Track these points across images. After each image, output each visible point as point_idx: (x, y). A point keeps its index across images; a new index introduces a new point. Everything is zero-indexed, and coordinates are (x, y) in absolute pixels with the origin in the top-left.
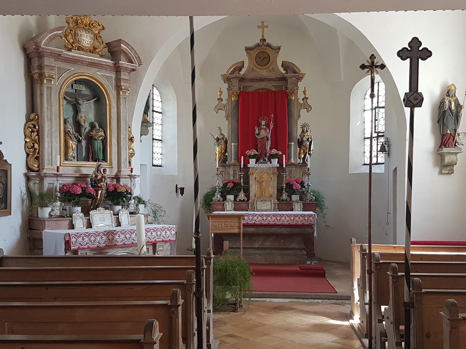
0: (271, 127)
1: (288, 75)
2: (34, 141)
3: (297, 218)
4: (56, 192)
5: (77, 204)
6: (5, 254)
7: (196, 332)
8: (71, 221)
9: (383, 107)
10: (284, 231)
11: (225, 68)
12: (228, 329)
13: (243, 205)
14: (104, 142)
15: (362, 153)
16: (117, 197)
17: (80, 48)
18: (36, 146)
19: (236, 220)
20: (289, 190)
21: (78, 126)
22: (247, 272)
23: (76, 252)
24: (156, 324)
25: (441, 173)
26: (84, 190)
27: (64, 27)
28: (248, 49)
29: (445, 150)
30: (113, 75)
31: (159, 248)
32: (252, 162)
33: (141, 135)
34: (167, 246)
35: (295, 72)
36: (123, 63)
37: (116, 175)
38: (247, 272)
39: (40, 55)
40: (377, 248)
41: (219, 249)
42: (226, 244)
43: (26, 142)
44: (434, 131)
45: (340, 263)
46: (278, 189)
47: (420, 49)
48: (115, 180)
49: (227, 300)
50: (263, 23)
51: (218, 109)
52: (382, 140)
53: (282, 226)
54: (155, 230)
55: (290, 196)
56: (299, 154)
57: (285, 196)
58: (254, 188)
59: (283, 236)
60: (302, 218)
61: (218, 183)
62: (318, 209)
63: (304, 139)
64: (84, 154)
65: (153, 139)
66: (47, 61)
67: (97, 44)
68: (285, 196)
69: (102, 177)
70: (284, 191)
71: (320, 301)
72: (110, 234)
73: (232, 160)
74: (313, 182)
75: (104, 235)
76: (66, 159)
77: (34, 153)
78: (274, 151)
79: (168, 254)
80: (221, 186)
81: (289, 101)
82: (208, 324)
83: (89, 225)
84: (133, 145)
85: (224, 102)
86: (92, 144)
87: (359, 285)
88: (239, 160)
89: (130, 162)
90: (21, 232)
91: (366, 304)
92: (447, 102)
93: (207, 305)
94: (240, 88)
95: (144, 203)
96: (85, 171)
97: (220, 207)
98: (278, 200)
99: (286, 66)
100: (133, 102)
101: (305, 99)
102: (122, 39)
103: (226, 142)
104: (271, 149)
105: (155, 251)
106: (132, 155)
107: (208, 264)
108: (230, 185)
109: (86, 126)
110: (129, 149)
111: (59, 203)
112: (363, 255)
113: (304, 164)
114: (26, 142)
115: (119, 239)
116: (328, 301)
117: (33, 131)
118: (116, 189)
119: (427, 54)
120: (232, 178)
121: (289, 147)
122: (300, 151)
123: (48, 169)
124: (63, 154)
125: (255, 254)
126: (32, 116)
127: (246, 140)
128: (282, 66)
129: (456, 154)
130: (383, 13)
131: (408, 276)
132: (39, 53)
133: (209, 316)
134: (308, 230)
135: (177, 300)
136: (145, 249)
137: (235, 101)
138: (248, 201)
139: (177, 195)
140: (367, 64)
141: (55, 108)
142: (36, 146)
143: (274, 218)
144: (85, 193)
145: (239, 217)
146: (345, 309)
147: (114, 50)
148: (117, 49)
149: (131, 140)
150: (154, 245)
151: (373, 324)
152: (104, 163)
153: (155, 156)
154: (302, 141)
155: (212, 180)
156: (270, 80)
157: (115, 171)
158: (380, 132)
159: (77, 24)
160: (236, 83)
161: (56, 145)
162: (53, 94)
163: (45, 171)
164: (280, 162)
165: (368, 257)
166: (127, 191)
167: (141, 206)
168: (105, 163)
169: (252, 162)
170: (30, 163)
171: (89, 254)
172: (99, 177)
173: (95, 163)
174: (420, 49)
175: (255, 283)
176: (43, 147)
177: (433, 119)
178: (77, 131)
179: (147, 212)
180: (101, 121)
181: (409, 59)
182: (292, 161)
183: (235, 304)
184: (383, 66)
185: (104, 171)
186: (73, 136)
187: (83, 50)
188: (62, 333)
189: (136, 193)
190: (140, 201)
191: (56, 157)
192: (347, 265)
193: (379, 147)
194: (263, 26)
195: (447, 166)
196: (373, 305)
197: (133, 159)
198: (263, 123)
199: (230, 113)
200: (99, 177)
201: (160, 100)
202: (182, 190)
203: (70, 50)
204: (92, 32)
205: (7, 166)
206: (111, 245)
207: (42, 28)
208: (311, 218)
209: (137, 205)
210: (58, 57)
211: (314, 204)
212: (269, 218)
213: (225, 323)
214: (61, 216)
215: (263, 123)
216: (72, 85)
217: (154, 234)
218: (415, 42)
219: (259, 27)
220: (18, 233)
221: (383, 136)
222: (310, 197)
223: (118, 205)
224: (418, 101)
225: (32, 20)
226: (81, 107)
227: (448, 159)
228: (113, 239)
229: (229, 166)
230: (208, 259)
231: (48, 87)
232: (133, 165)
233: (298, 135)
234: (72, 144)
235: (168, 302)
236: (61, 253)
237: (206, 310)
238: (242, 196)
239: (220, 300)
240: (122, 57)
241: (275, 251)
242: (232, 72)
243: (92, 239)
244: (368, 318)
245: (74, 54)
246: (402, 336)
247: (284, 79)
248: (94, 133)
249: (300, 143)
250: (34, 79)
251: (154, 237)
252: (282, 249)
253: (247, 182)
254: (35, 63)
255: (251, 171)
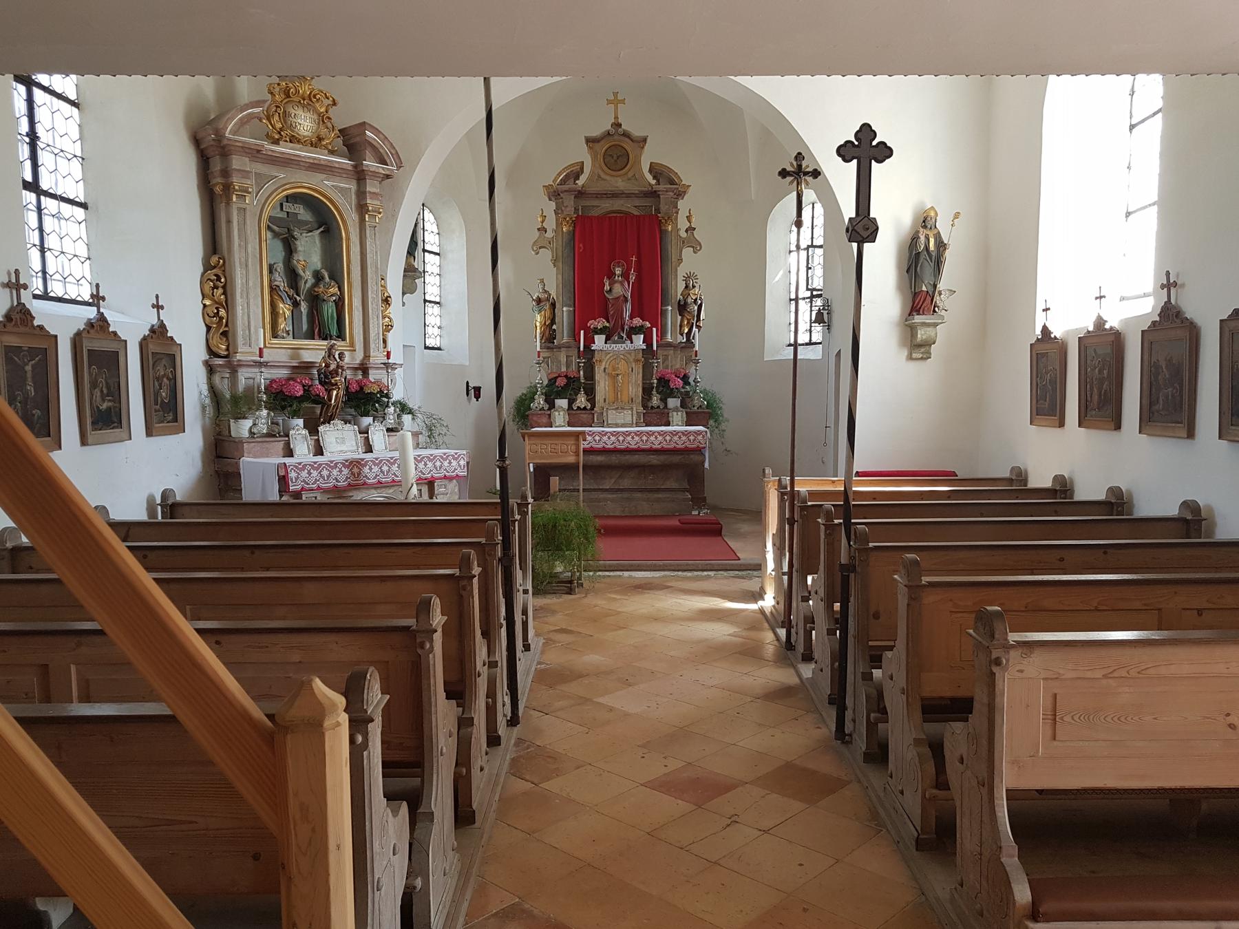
0: (632, 278)
1: (661, 187)
2: (218, 305)
3: (676, 438)
4: (259, 392)
5: (296, 414)
6: (178, 498)
7: (504, 623)
8: (288, 444)
9: (821, 247)
10: (654, 459)
11: (551, 174)
12: (559, 620)
13: (585, 416)
14: (339, 304)
15: (788, 326)
16: (365, 401)
17: (294, 139)
18: (222, 312)
19: (572, 441)
20: (662, 390)
21: (293, 276)
22: (591, 529)
23: (297, 495)
24: (436, 603)
25: (910, 358)
26: (307, 389)
27: (265, 101)
28: (590, 141)
29: (918, 319)
30: (353, 186)
31: (438, 489)
32: (599, 340)
33: (404, 294)
34: (453, 486)
35: (672, 182)
36: (370, 164)
37: (362, 364)
38: (591, 529)
39: (225, 152)
40: (804, 483)
41: (542, 491)
42: (555, 481)
43: (205, 306)
44: (900, 288)
45: (745, 512)
46: (644, 389)
47: (874, 143)
48: (360, 372)
49: (556, 575)
50: (615, 94)
51: (538, 247)
52: (818, 302)
53: (651, 451)
54: (432, 458)
55: (664, 400)
56: (681, 326)
57: (655, 401)
58: (602, 387)
59: (652, 469)
60: (684, 438)
61: (540, 378)
62: (711, 422)
63: (689, 300)
64: (305, 327)
65: (425, 301)
66: (237, 162)
67: (323, 132)
68: (655, 401)
69: (338, 366)
70: (654, 392)
71: (712, 573)
72: (355, 465)
73: (564, 337)
74: (703, 376)
75: (344, 466)
76: (275, 336)
77: (220, 324)
78: (637, 321)
79: (455, 499)
80: (546, 382)
81: (663, 233)
82: (525, 612)
83: (319, 451)
84: (391, 309)
85: (550, 234)
86: (319, 310)
87: (774, 545)
88: (576, 337)
89: (385, 341)
90: (203, 462)
91: (784, 574)
92: (922, 238)
93: (523, 581)
94: (576, 210)
95: (410, 412)
96: (307, 357)
97: (545, 420)
98: (645, 407)
99: (657, 171)
100: (390, 232)
101: (690, 229)
102: (1189, 441)
103: (553, 305)
104: (631, 317)
105: (432, 493)
106: (388, 328)
107: (524, 514)
108: (561, 382)
109: (307, 278)
110: (384, 318)
111: (264, 412)
112: (783, 494)
113: (689, 343)
114: (205, 306)
115: (371, 473)
116: (725, 574)
117: (215, 287)
118: (362, 388)
119: (884, 152)
120: (564, 369)
121: (664, 313)
122: (682, 321)
123: (244, 353)
124: (268, 326)
125: (606, 500)
126: (214, 260)
127: (588, 303)
128: (650, 171)
129: (935, 325)
130: (821, 79)
131: (848, 525)
132: (223, 147)
133: (525, 597)
134: (695, 458)
135: (470, 568)
136: (415, 490)
137: (569, 232)
138: (592, 409)
139: (469, 400)
140: (789, 169)
141: (253, 246)
142: (222, 312)
143: (637, 438)
144: (308, 395)
145: (577, 435)
146: (752, 585)
147: (353, 142)
148: (358, 139)
149: (387, 301)
150: (431, 484)
151: (794, 604)
152: (339, 343)
153: (429, 330)
154: (686, 303)
155: (528, 373)
156: (629, 196)
157: (359, 356)
158: (815, 289)
159: (287, 95)
160: (569, 201)
161: (256, 310)
162: (248, 222)
163: (239, 357)
164: (648, 341)
165: (789, 497)
166: (381, 392)
167: (407, 418)
168: (342, 343)
169: (599, 340)
170: (213, 342)
171: (321, 498)
172: (333, 367)
173: (325, 343)
174: (874, 143)
175: (602, 546)
176: (234, 315)
177: (899, 267)
178: (291, 287)
179: (416, 429)
180: (333, 267)
181: (855, 161)
182: (669, 338)
183: (571, 582)
184: (816, 173)
185: (341, 355)
186: (284, 295)
187: (299, 141)
188: (284, 618)
189: (397, 394)
190: (403, 408)
191: (257, 332)
192: (758, 515)
193: (814, 314)
194: (616, 101)
195: (920, 346)
196: (795, 574)
197: (390, 336)
198: (618, 271)
199: (560, 254)
200: (333, 367)
201: (436, 231)
202: (477, 390)
203: (276, 142)
204: (315, 111)
205: (175, 348)
206: (358, 483)
207: (227, 103)
208: (700, 437)
209: (399, 416)
210: (255, 154)
211: (705, 413)
212: (629, 438)
213: (554, 612)
214: (269, 435)
215: (618, 271)
216: (281, 205)
217: (430, 465)
218: (866, 131)
219: (609, 102)
220: (198, 464)
221: (819, 296)
222: (698, 401)
223: (367, 415)
224: (869, 232)
225: (206, 85)
226: (298, 243)
227: (921, 334)
228: (359, 474)
229: (559, 347)
230: (523, 506)
231: (239, 209)
232: (390, 346)
233: (679, 293)
234: (285, 308)
235: (456, 572)
236: (274, 496)
237: (521, 589)
238: (582, 400)
239: (545, 576)
240: (368, 154)
241: (639, 495)
242: (563, 182)
243: (325, 473)
244: (787, 596)
245: (284, 149)
246: (837, 621)
247: (653, 194)
248: (321, 289)
249: (682, 308)
250: (215, 193)
251: (429, 470)
252: (651, 491)
253: (590, 375)
254: (216, 166)
255: (597, 356)
